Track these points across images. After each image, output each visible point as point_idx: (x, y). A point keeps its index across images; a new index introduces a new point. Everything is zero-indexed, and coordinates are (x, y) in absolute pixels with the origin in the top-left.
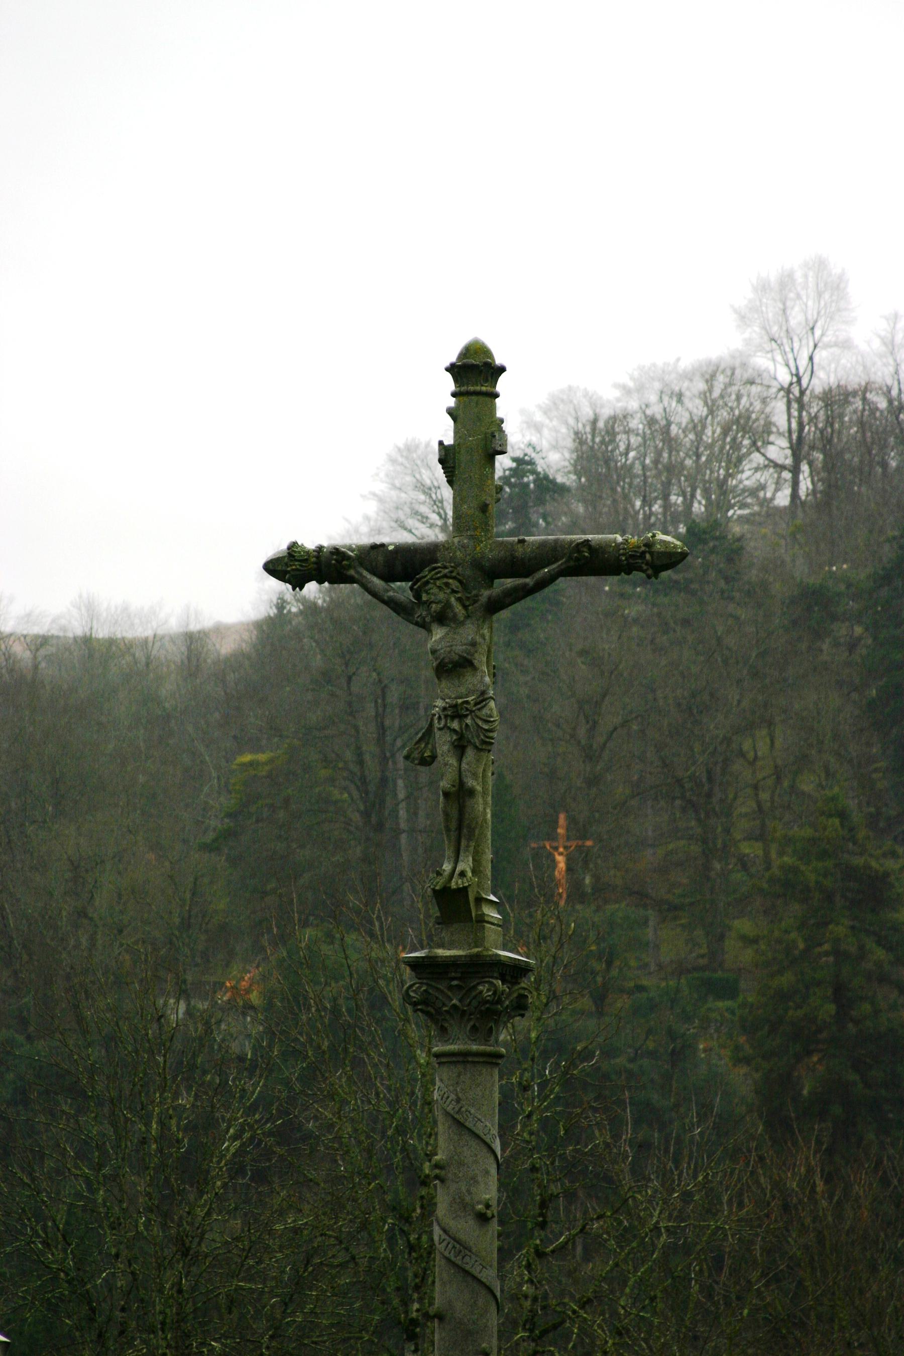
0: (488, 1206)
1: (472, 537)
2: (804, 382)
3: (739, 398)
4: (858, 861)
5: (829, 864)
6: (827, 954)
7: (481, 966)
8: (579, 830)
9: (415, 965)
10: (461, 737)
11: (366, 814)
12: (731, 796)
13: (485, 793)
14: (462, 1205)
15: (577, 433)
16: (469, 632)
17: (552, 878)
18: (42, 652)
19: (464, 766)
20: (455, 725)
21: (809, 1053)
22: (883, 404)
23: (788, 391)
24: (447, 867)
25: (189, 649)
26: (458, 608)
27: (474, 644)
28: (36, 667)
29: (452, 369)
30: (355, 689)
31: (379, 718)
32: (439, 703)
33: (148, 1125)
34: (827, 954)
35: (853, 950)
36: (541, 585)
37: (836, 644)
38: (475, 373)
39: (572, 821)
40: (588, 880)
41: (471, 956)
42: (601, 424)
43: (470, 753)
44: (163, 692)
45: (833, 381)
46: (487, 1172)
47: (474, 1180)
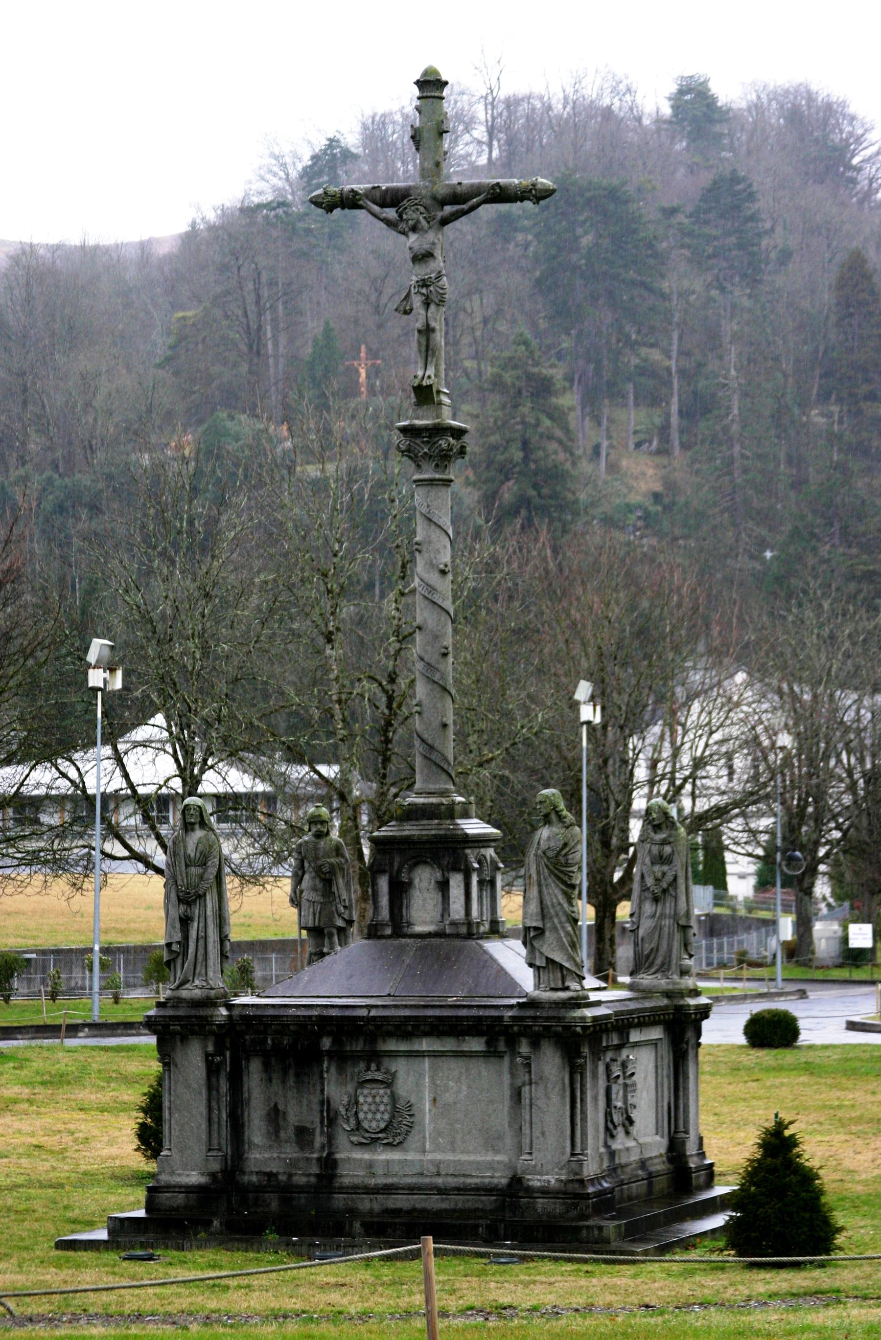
0: (446, 566)
1: (430, 181)
2: (495, 94)
3: (456, 102)
4: (536, 370)
5: (519, 372)
6: (517, 423)
7: (439, 430)
8: (373, 354)
9: (404, 430)
10: (427, 297)
11: (250, 347)
12: (459, 334)
13: (441, 330)
14: (432, 565)
15: (363, 124)
16: (431, 236)
17: (358, 381)
18: (58, 253)
19: (429, 314)
20: (424, 291)
21: (509, 480)
22: (538, 105)
23: (486, 98)
24: (420, 373)
25: (143, 252)
26: (424, 223)
27: (434, 244)
28: (54, 262)
29: (417, 83)
30: (242, 273)
31: (257, 290)
32: (415, 278)
33: (181, 523)
34: (517, 423)
35: (533, 421)
36: (473, 208)
37: (517, 246)
38: (431, 85)
39: (369, 350)
40: (378, 383)
41: (435, 425)
42: (377, 118)
43: (433, 307)
44: (127, 277)
45: (511, 93)
46: (445, 547)
47: (438, 551)
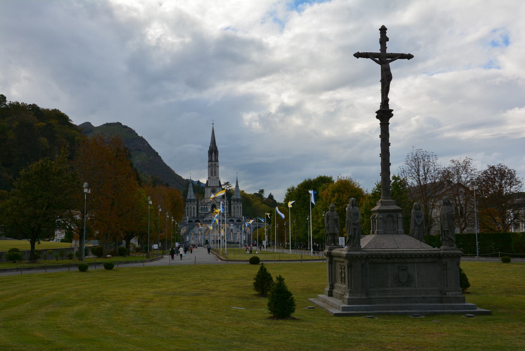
38: (383, 30)
